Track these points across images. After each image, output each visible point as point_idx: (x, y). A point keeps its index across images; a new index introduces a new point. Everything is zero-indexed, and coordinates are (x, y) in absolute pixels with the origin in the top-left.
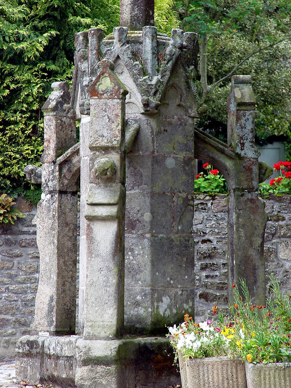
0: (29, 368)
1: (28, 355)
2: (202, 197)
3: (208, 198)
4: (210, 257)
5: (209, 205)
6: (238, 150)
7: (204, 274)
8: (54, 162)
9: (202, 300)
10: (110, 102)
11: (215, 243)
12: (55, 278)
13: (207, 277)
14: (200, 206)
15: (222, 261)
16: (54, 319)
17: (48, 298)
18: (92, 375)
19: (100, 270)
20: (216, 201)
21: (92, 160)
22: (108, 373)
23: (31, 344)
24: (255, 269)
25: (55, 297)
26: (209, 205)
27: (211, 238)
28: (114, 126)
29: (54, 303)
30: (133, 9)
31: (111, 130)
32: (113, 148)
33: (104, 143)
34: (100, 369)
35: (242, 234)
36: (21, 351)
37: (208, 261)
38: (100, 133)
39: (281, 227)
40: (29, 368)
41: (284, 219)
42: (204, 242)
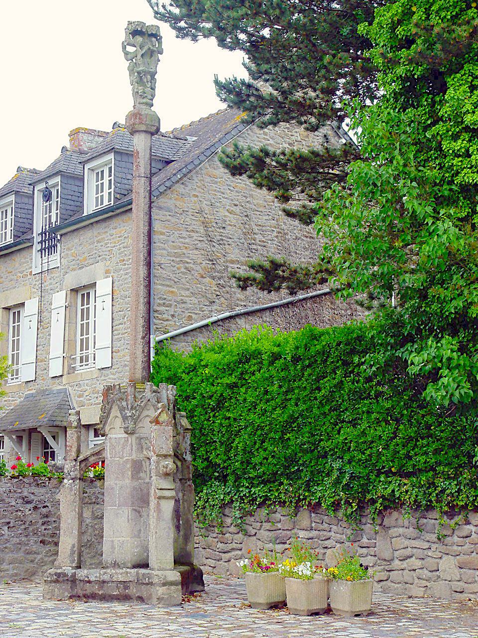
0: (56, 590)
1: (57, 581)
2: (43, 478)
3: (47, 479)
4: (47, 516)
5: (47, 483)
6: (184, 457)
7: (43, 527)
8: (76, 460)
9: (42, 544)
10: (166, 428)
11: (50, 508)
12: (77, 533)
13: (45, 529)
14: (43, 485)
15: (54, 519)
16: (76, 559)
17: (70, 546)
18: (169, 591)
19: (165, 529)
20: (51, 481)
21: (158, 462)
22: (177, 590)
23: (58, 575)
24: (191, 526)
25: (76, 545)
26: (47, 483)
27: (48, 505)
28: (168, 442)
29: (75, 549)
30: (143, 371)
31: (167, 445)
32: (170, 455)
33: (164, 453)
34: (173, 588)
35: (186, 506)
36: (49, 579)
37: (45, 519)
38: (161, 446)
39: (86, 497)
40: (56, 590)
41: (87, 493)
42: (44, 507)
